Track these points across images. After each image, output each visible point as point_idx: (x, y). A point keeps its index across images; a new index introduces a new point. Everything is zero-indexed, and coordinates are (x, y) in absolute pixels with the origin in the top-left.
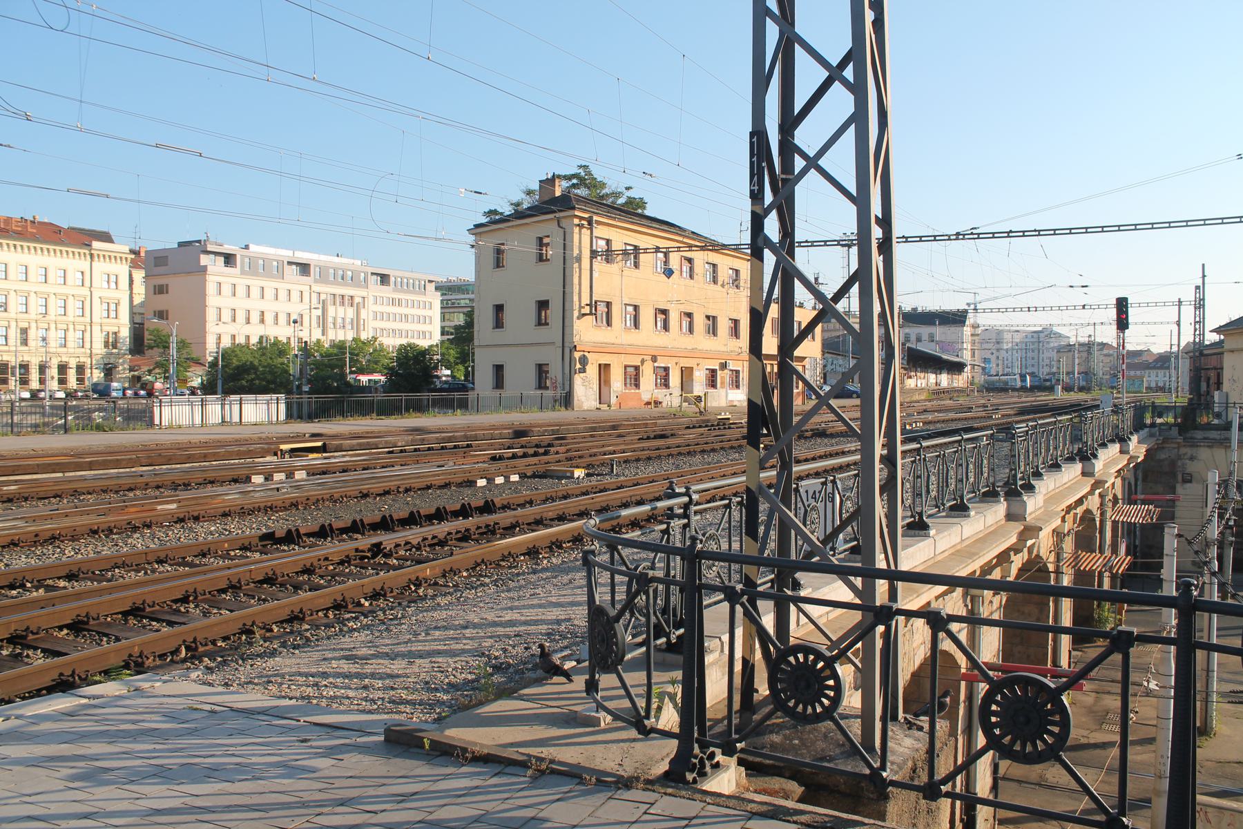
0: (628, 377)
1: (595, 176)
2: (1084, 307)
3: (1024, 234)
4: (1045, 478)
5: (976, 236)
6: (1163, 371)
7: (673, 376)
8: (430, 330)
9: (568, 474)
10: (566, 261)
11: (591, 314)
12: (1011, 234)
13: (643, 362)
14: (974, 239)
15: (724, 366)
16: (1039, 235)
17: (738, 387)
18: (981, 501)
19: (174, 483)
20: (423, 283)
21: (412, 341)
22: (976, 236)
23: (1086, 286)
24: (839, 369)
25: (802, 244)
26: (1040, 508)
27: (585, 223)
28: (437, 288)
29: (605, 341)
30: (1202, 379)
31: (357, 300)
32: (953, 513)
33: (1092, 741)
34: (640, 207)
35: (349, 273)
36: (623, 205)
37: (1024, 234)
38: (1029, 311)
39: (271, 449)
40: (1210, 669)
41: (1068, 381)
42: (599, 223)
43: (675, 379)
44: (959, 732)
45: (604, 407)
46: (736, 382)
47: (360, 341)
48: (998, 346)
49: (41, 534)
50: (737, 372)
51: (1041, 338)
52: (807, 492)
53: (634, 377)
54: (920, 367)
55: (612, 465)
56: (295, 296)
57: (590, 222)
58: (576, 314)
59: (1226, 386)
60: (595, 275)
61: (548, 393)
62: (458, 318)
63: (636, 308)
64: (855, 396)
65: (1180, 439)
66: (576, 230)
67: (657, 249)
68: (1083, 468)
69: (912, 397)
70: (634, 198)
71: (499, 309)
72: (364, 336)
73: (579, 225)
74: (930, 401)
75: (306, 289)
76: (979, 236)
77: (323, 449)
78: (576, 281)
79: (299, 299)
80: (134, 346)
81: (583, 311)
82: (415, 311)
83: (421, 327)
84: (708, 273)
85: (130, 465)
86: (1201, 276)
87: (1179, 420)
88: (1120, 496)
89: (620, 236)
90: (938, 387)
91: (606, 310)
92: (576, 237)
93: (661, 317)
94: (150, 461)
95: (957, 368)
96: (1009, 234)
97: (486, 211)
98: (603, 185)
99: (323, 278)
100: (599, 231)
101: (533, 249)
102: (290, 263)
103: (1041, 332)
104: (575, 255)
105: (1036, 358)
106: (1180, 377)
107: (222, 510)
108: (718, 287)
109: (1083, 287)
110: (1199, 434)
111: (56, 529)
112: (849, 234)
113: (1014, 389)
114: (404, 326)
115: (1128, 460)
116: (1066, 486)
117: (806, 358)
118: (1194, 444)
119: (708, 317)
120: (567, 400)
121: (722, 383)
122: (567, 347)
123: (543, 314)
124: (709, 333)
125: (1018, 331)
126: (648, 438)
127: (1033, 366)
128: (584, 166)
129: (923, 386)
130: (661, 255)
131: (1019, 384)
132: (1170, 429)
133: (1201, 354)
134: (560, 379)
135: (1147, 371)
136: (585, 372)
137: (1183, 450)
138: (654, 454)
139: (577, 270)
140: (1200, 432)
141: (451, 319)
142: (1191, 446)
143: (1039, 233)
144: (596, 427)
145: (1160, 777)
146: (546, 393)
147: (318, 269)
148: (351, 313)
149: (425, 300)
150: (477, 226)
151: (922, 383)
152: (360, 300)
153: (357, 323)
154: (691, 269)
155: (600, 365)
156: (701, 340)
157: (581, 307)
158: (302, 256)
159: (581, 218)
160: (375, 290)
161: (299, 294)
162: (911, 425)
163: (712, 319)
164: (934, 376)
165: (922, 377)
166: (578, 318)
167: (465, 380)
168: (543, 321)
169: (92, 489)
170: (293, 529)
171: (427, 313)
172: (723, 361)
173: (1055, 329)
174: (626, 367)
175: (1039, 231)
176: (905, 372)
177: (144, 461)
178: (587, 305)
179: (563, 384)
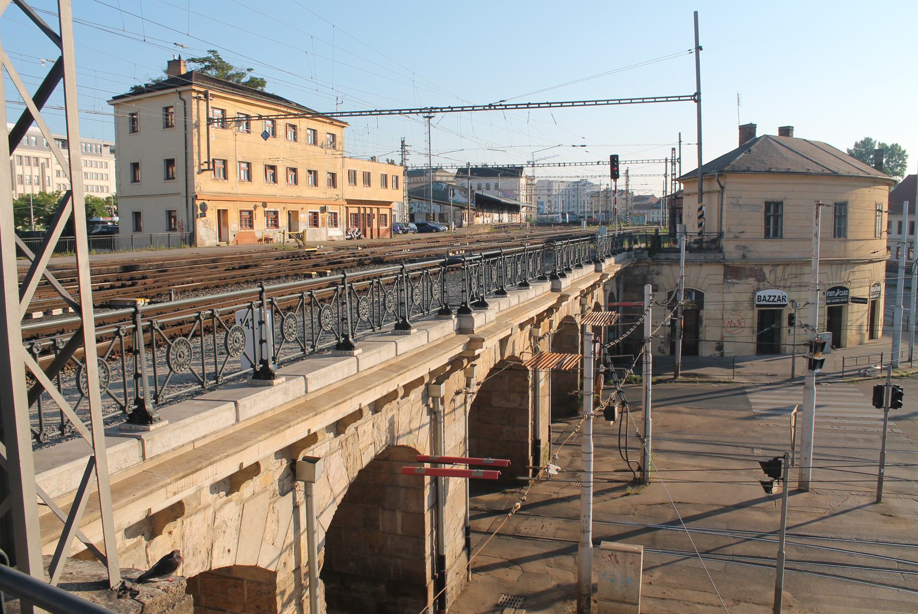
0: (244, 219)
1: (223, 60)
2: (598, 163)
3: (539, 105)
4: (508, 296)
5: (504, 107)
8: (106, 185)
11: (209, 169)
12: (529, 106)
13: (255, 207)
14: (502, 109)
15: (324, 210)
16: (550, 107)
17: (336, 226)
18: (436, 318)
20: (99, 146)
21: (92, 194)
22: (504, 107)
23: (585, 146)
24: (424, 211)
25: (373, 113)
26: (492, 321)
27: (202, 96)
29: (223, 191)
30: (677, 215)
31: (41, 161)
33: (561, 496)
34: (260, 85)
36: (245, 84)
37: (539, 105)
38: (559, 164)
40: (647, 435)
41: (596, 218)
43: (283, 221)
44: (426, 508)
47: (46, 194)
48: (549, 193)
50: (335, 214)
53: (248, 220)
55: (171, 295)
58: (196, 169)
60: (212, 139)
61: (177, 234)
63: (249, 164)
64: (434, 230)
65: (649, 260)
66: (195, 102)
68: (552, 285)
69: (477, 231)
70: (256, 78)
72: (49, 190)
73: (196, 98)
74: (493, 233)
76: (506, 107)
78: (195, 143)
81: (202, 167)
82: (94, 170)
84: (309, 137)
87: (649, 245)
88: (602, 303)
89: (234, 107)
90: (501, 223)
91: (223, 166)
92: (194, 106)
93: (270, 172)
95: (514, 209)
97: (133, 87)
98: (231, 68)
100: (214, 103)
101: (160, 115)
103: (578, 182)
104: (194, 122)
105: (576, 202)
106: (662, 215)
108: (317, 149)
109: (582, 146)
110: (663, 256)
113: (558, 224)
115: (601, 277)
116: (533, 300)
118: (658, 263)
120: (191, 239)
121: (323, 223)
122: (190, 196)
123: (171, 171)
125: (562, 182)
126: (234, 269)
127: (574, 207)
129: (489, 222)
131: (561, 220)
132: (643, 252)
134: (185, 223)
135: (652, 210)
136: (205, 216)
137: (652, 268)
138: (223, 282)
139: (197, 134)
140: (663, 254)
142: (657, 265)
143: (550, 105)
144: (197, 261)
145: (584, 532)
146: (173, 234)
148: (36, 171)
150: (115, 98)
152: (44, 161)
153: (42, 180)
154: (295, 134)
155: (219, 211)
156: (305, 190)
157: (200, 164)
159: (199, 92)
162: (454, 252)
163: (314, 173)
164: (497, 215)
165: (488, 215)
166: (198, 173)
168: (171, 176)
172: (323, 206)
173: (590, 180)
174: (241, 211)
175: (550, 103)
176: (474, 212)
179: (188, 227)
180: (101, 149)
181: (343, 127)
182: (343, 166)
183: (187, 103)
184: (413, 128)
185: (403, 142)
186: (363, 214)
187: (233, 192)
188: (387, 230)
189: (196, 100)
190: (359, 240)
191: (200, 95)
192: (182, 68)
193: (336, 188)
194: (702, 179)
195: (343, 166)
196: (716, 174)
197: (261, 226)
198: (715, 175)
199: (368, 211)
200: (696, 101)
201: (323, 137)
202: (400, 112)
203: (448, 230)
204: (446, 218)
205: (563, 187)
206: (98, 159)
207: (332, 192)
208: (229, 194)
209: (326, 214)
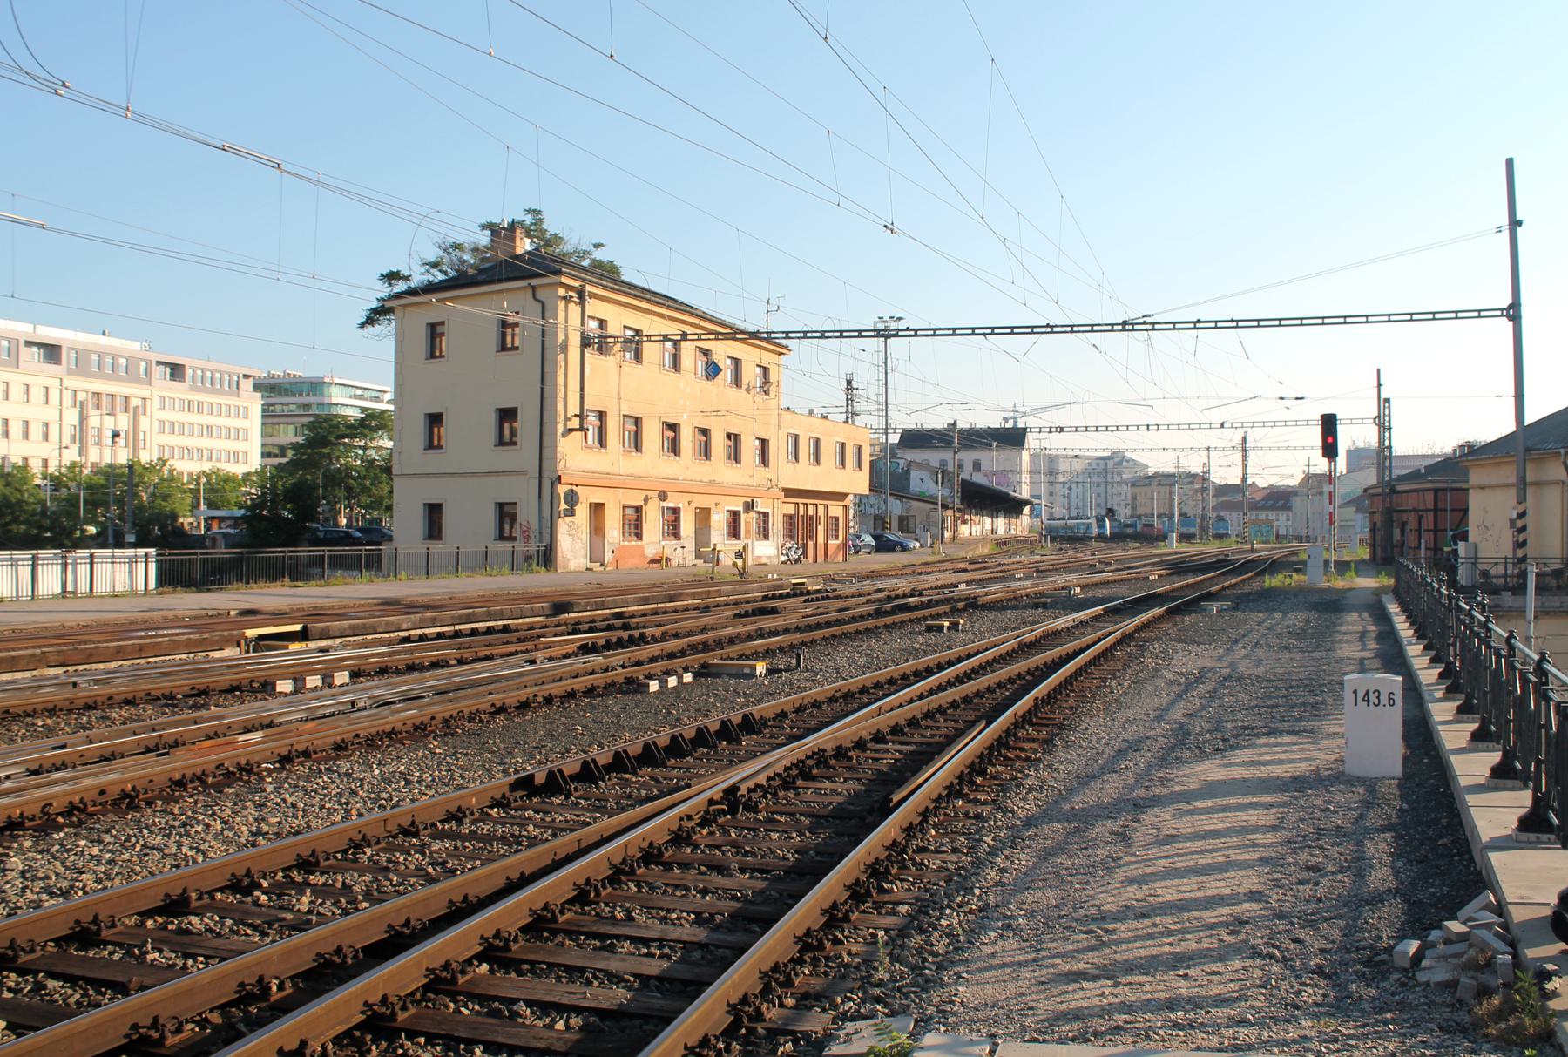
0: (627, 522)
2: (1062, 429)
3: (1216, 325)
6: (1285, 512)
7: (685, 521)
9: (747, 671)
10: (546, 350)
12: (1198, 325)
13: (646, 500)
14: (1147, 330)
15: (749, 506)
16: (1237, 327)
17: (766, 537)
19: (148, 694)
20: (235, 378)
21: (220, 465)
22: (1150, 327)
28: (257, 387)
29: (598, 469)
31: (135, 402)
32: (1465, 716)
35: (123, 361)
37: (1216, 325)
38: (1148, 430)
39: (233, 636)
41: (1160, 526)
42: (592, 295)
43: (687, 526)
45: (596, 567)
46: (764, 529)
49: (108, 790)
50: (766, 515)
51: (1109, 467)
52: (1355, 692)
53: (635, 526)
54: (975, 507)
56: (37, 394)
57: (581, 294)
58: (560, 429)
59: (1473, 535)
62: (286, 432)
64: (898, 548)
66: (562, 304)
67: (666, 338)
69: (974, 550)
71: (435, 420)
72: (145, 458)
73: (565, 298)
75: (54, 384)
77: (304, 635)
79: (42, 399)
80: (1415, 475)
81: (570, 425)
83: (232, 445)
85: (32, 666)
86: (1376, 384)
89: (619, 319)
91: (599, 423)
92: (561, 315)
94: (61, 659)
95: (1010, 506)
96: (1196, 324)
97: (384, 273)
99: (82, 365)
100: (594, 307)
102: (29, 344)
105: (1103, 495)
107: (331, 740)
108: (742, 392)
109: (1297, 399)
111: (125, 781)
112: (886, 318)
114: (205, 443)
117: (847, 495)
119: (729, 436)
120: (547, 557)
121: (747, 532)
122: (546, 478)
124: (730, 458)
128: (534, 211)
130: (669, 344)
131: (1095, 531)
133: (1393, 491)
134: (534, 525)
139: (563, 363)
141: (275, 433)
143: (1236, 324)
147: (73, 354)
149: (237, 403)
151: (976, 530)
157: (567, 419)
158: (50, 334)
159: (569, 287)
160: (164, 385)
161: (42, 390)
164: (990, 519)
166: (564, 435)
167: (347, 527)
169: (32, 708)
170: (555, 769)
171: (240, 423)
172: (749, 500)
175: (1237, 321)
177: (53, 659)
178: (576, 416)
180: (238, 382)
181: (781, 354)
182: (780, 427)
183: (548, 307)
184: (862, 359)
185: (849, 382)
186: (803, 516)
187: (613, 471)
188: (839, 546)
189: (564, 301)
190: (798, 565)
191: (571, 293)
192: (518, 242)
193: (768, 466)
194: (1525, 460)
195: (780, 427)
196: (1562, 451)
197: (654, 539)
198: (1559, 453)
199: (811, 512)
200: (1510, 318)
201: (750, 374)
202: (973, 331)
203: (918, 550)
204: (911, 526)
205: (1078, 466)
206: (233, 401)
207: (762, 475)
208: (608, 474)
209: (752, 514)
